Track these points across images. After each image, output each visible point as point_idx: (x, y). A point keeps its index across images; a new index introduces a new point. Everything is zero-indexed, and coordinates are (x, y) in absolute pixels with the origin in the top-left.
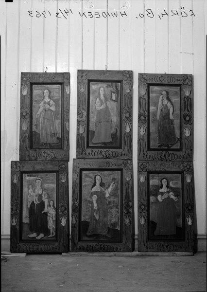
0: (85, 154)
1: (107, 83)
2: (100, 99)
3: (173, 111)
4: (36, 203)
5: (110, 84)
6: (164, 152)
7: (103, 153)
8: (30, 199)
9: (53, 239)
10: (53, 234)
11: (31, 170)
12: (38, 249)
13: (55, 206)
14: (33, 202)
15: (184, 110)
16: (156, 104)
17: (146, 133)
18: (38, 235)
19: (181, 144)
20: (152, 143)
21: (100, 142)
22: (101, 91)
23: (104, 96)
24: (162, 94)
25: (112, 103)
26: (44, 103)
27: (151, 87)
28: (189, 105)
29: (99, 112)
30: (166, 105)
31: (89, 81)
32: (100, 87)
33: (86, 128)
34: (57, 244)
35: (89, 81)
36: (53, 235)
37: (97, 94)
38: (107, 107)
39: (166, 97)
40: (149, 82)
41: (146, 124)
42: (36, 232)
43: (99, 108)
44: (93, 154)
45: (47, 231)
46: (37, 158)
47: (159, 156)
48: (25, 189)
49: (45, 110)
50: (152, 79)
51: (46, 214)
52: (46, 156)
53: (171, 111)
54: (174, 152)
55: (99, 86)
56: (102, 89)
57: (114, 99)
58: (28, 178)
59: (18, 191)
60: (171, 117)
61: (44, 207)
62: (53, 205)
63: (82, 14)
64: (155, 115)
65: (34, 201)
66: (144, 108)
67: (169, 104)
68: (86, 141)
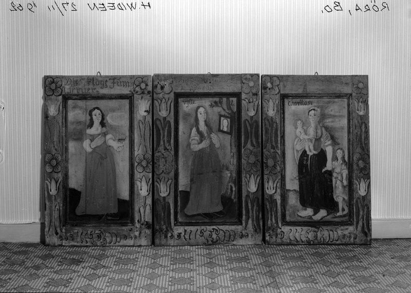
0: (172, 236)
1: (211, 99)
2: (198, 130)
4: (310, 154)
5: (217, 99)
7: (207, 234)
8: (299, 147)
9: (344, 219)
10: (343, 210)
11: (300, 91)
12: (316, 237)
13: (346, 159)
14: (305, 152)
18: (315, 213)
21: (200, 211)
22: (199, 115)
23: (207, 124)
25: (221, 135)
29: (200, 155)
32: (198, 108)
33: (173, 186)
34: (351, 228)
35: (178, 96)
36: (345, 213)
37: (192, 120)
38: (212, 145)
40: (287, 91)
42: (311, 206)
43: (196, 147)
44: (187, 237)
45: (332, 205)
48: (289, 128)
51: (330, 173)
56: (201, 110)
57: (225, 129)
58: (293, 107)
59: (277, 130)
61: (325, 160)
62: (343, 157)
63: (92, 6)
65: (307, 149)
68: (172, 211)
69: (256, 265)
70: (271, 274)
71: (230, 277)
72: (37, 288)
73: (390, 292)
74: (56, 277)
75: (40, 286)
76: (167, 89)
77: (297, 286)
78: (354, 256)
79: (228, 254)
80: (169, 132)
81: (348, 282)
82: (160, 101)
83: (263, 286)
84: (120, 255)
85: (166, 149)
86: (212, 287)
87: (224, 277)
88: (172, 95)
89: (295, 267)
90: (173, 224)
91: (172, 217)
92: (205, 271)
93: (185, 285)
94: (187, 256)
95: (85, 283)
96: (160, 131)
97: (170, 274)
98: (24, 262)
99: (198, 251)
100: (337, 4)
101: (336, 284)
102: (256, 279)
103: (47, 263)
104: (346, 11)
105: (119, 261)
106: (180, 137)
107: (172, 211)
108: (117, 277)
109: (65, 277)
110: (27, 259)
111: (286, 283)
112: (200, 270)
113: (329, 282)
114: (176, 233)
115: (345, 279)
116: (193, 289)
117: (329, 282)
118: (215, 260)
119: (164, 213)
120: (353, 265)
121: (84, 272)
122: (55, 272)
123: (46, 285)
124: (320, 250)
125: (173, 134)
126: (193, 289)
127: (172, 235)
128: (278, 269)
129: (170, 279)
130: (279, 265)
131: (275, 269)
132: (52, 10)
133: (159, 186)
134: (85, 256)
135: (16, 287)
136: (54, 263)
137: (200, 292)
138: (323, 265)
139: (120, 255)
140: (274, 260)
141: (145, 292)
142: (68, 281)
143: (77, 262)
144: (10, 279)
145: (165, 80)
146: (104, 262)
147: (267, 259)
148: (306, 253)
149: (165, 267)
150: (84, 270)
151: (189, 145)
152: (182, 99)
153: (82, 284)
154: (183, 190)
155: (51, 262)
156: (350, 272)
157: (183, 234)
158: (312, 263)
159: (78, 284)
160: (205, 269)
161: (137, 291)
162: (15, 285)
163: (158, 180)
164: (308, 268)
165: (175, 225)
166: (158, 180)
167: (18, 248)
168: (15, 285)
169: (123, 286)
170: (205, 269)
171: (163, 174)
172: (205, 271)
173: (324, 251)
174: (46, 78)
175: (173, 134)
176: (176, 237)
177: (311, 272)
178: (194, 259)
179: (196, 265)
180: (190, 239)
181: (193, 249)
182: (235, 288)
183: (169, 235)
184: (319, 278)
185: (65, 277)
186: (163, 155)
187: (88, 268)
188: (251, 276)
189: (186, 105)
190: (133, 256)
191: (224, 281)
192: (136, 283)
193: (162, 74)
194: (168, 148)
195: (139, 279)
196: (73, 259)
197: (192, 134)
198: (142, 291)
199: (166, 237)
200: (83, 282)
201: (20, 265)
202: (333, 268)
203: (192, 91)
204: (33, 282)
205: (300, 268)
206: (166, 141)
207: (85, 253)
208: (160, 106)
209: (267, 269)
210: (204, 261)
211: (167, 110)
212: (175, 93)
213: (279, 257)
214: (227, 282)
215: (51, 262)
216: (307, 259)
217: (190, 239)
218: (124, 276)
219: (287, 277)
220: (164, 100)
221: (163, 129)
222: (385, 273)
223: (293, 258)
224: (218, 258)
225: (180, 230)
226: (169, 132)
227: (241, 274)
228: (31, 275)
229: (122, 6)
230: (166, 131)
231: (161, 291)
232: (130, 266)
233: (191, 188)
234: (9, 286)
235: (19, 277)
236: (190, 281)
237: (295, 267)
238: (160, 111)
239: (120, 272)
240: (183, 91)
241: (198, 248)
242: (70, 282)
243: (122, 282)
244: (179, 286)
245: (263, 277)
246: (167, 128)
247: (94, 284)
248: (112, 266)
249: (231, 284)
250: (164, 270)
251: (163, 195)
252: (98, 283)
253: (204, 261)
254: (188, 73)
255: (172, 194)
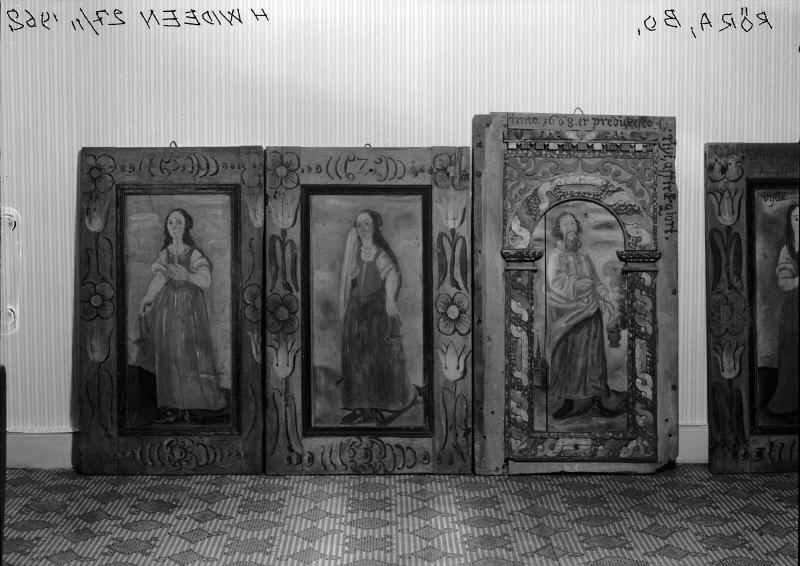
0: (747, 455)
3: (399, 287)
6: (365, 439)
15: (441, 283)
16: (336, 267)
17: (298, 371)
19: (429, 411)
20: (319, 406)
24: (355, 225)
26: (170, 260)
27: (316, 200)
28: (457, 262)
30: (372, 265)
31: (752, 185)
33: (746, 357)
37: (781, 233)
39: (370, 235)
40: (313, 179)
41: (298, 335)
44: (775, 454)
46: (145, 464)
47: (346, 456)
49: (171, 284)
50: (318, 167)
52: (177, 456)
53: (390, 287)
54: (404, 441)
55: (787, 203)
60: (391, 307)
64: (328, 307)
66: (289, 279)
67: (383, 262)
68: (746, 407)
69: (512, 513)
70: (542, 531)
71: (345, 537)
72: (90, 556)
73: (432, 565)
74: (127, 535)
75: (96, 553)
76: (733, 171)
77: (592, 554)
78: (703, 497)
79: (354, 494)
80: (738, 255)
81: (690, 545)
82: (718, 195)
83: (525, 554)
84: (250, 493)
85: (731, 287)
86: (428, 555)
87: (450, 536)
88: (743, 184)
89: (589, 517)
90: (747, 432)
91: (746, 418)
92: (414, 525)
93: (376, 552)
94: (380, 496)
95: (182, 548)
96: (719, 252)
97: (345, 531)
98: (64, 507)
99: (400, 487)
100: (671, 16)
101: (670, 552)
102: (629, 539)
103: (109, 508)
104: (686, 27)
105: (245, 508)
106: (758, 264)
107: (746, 407)
108: (244, 536)
109: (143, 536)
110: (70, 500)
111: (571, 547)
112: (405, 523)
113: (655, 547)
114: (753, 448)
115: (687, 540)
116: (391, 560)
117: (655, 547)
118: (434, 505)
119: (731, 411)
120: (701, 515)
121: (181, 526)
122: (124, 527)
123: (107, 550)
124: (637, 486)
125: (744, 260)
126: (391, 560)
127: (747, 452)
128: (555, 523)
129: (347, 540)
130: (557, 514)
131: (549, 522)
132: (85, 28)
133: (719, 358)
134: (182, 496)
135: (49, 555)
136: (122, 509)
137: (529, 564)
138: (643, 513)
139: (250, 493)
140: (547, 504)
141: (298, 565)
142: (150, 544)
143: (167, 507)
144: (38, 539)
145: (729, 155)
146: (218, 507)
147: (534, 502)
148: (610, 491)
149: (336, 516)
150: (180, 521)
151: (775, 279)
152: (761, 191)
153: (176, 550)
154: (765, 365)
155: (116, 507)
156: (695, 527)
157: (768, 450)
158: (622, 510)
159: (170, 549)
160: (414, 521)
161: (283, 563)
162: (49, 551)
163: (718, 348)
164: (614, 519)
165: (751, 432)
166: (718, 348)
167: (54, 480)
168: (49, 551)
169: (255, 554)
170: (414, 521)
171: (727, 336)
172: (414, 525)
173: (644, 487)
174: (85, 153)
175: (744, 260)
176: (754, 456)
177: (621, 528)
178: (393, 502)
179: (396, 511)
180: (780, 459)
181: (390, 482)
182: (472, 558)
183: (742, 452)
184: (636, 539)
185: (143, 536)
186: (727, 299)
187: (188, 518)
188: (503, 535)
189: (769, 203)
190: (274, 496)
191: (451, 544)
192: (281, 546)
193: (724, 144)
194: (736, 285)
195: (286, 540)
196: (159, 501)
197: (782, 259)
198: (169, 563)
199: (735, 455)
200: (179, 546)
201: (58, 512)
202: (661, 519)
203: (780, 176)
204: (82, 546)
205: (598, 520)
206: (731, 272)
207: (183, 490)
208: (719, 204)
209: (532, 522)
210: (412, 506)
211: (733, 213)
212: (747, 179)
213: (557, 500)
214: (457, 546)
215: (116, 507)
216: (611, 502)
217: (780, 459)
218: (258, 535)
219: (572, 535)
220: (726, 194)
221: (726, 249)
222: (764, 530)
223: (584, 501)
224: (439, 500)
225: (762, 442)
226: (738, 255)
227: (484, 532)
228: (77, 531)
229: (213, 17)
230: (732, 252)
231: (336, 563)
232: (270, 516)
233: (779, 363)
234: (36, 552)
235: (55, 534)
236: (386, 544)
237: (589, 517)
238: (720, 214)
239: (250, 526)
240: (763, 176)
241: (400, 481)
242: (36, 545)
243: (253, 546)
244: (364, 553)
245: (526, 536)
246: (733, 248)
247: (199, 550)
248: (234, 516)
249: (344, 552)
250: (335, 523)
251: (727, 375)
252: (207, 547)
253: (412, 506)
254: (754, 142)
255: (745, 374)
